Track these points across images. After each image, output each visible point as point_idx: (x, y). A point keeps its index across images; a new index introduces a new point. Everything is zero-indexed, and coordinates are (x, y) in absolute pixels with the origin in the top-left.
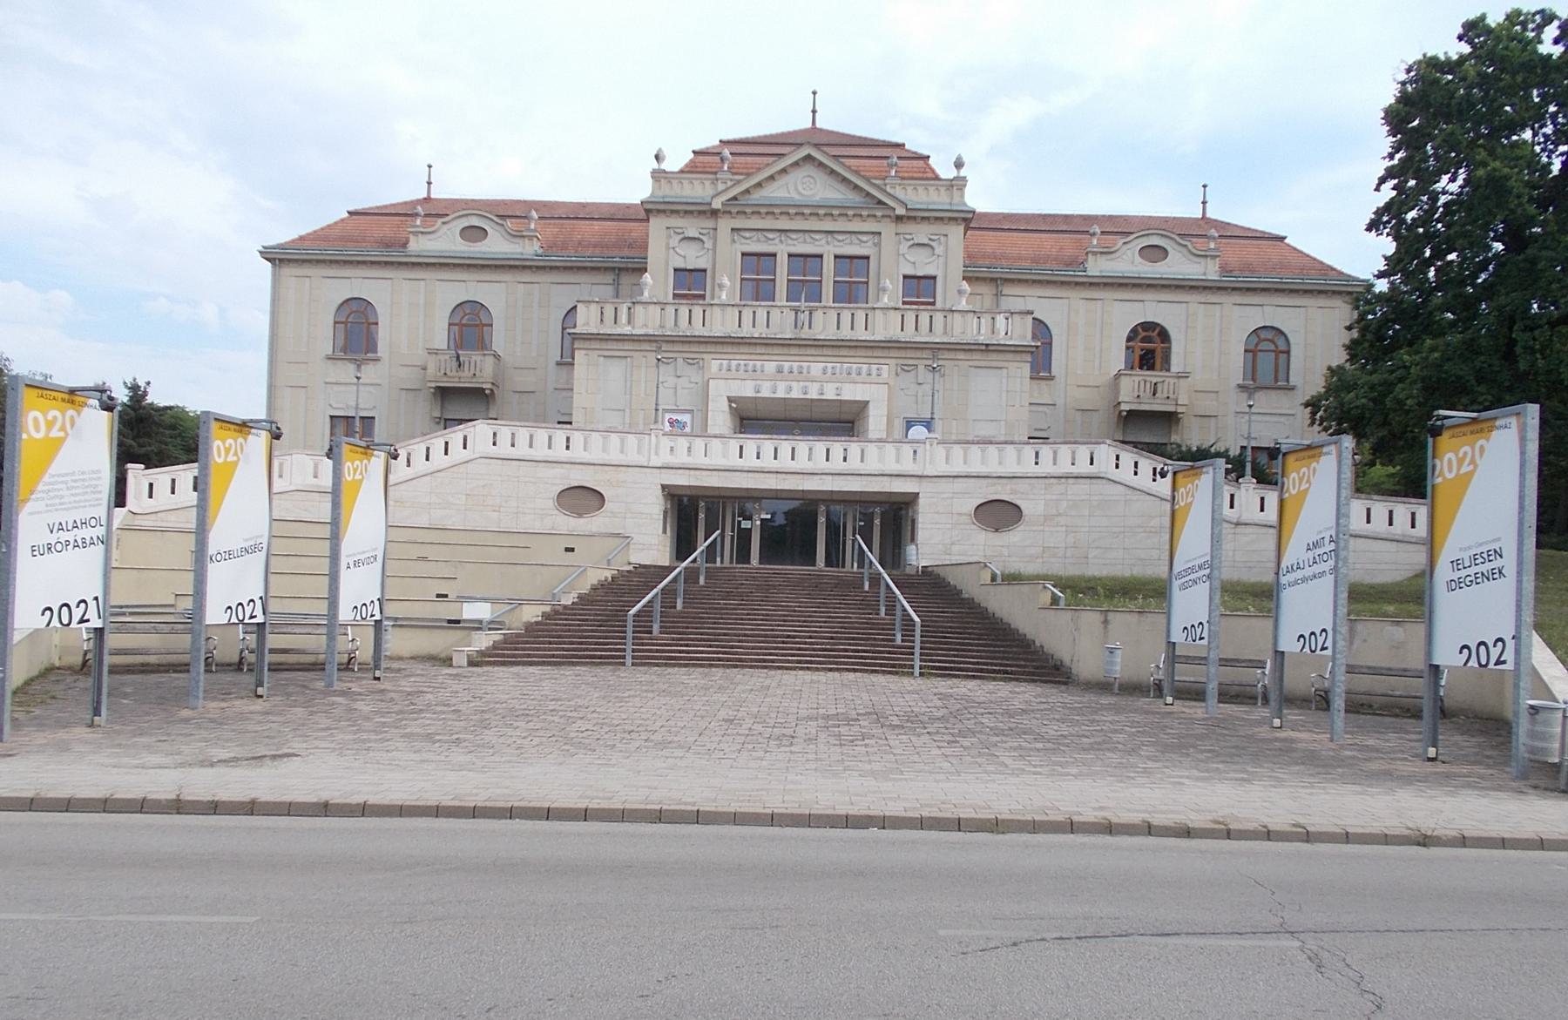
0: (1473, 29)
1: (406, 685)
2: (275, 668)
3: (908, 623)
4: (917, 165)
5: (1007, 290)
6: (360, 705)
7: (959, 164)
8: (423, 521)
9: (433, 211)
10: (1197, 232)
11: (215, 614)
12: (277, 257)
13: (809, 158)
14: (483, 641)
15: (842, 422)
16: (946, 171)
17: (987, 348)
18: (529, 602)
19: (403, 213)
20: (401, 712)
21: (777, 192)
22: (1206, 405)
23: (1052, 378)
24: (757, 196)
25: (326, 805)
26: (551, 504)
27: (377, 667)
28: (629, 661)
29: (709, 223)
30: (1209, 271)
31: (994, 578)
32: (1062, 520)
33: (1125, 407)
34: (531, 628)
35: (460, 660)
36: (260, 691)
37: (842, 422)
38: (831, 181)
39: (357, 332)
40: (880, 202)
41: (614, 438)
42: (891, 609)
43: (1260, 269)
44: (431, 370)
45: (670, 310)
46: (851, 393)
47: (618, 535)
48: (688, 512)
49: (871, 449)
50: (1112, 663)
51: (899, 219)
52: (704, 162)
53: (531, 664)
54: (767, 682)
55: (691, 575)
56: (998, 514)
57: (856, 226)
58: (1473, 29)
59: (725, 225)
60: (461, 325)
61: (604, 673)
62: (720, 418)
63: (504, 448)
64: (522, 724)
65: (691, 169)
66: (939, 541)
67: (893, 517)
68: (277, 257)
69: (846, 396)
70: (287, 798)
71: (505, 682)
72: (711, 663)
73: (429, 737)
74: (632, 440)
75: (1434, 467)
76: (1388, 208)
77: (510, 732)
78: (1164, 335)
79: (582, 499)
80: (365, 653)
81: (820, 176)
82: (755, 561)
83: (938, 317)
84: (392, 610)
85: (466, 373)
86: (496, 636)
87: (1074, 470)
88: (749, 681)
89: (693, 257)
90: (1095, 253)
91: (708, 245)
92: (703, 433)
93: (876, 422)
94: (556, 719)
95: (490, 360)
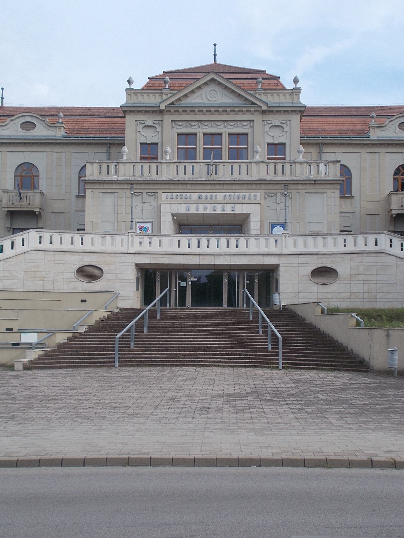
3: (275, 339)
4: (273, 82)
7: (296, 81)
14: (33, 355)
15: (235, 226)
16: (289, 85)
17: (315, 182)
21: (196, 99)
22: (57, 206)
23: (352, 197)
24: (184, 102)
28: (117, 364)
29: (159, 118)
30: (59, 134)
31: (323, 311)
33: (394, 212)
34: (61, 347)
35: (19, 366)
37: (235, 226)
40: (253, 103)
42: (265, 330)
45: (138, 166)
47: (111, 292)
48: (150, 278)
49: (252, 240)
50: (392, 360)
51: (264, 112)
52: (155, 84)
53: (60, 368)
54: (196, 374)
55: (152, 314)
56: (324, 275)
57: (240, 117)
59: (167, 118)
61: (103, 372)
62: (167, 225)
63: (46, 245)
64: (52, 405)
65: (148, 88)
66: (291, 290)
67: (265, 278)
71: (44, 378)
72: (163, 364)
77: (44, 410)
79: (90, 272)
85: (25, 203)
86: (40, 352)
89: (150, 137)
90: (374, 127)
91: (159, 129)
93: (254, 225)
95: (38, 196)
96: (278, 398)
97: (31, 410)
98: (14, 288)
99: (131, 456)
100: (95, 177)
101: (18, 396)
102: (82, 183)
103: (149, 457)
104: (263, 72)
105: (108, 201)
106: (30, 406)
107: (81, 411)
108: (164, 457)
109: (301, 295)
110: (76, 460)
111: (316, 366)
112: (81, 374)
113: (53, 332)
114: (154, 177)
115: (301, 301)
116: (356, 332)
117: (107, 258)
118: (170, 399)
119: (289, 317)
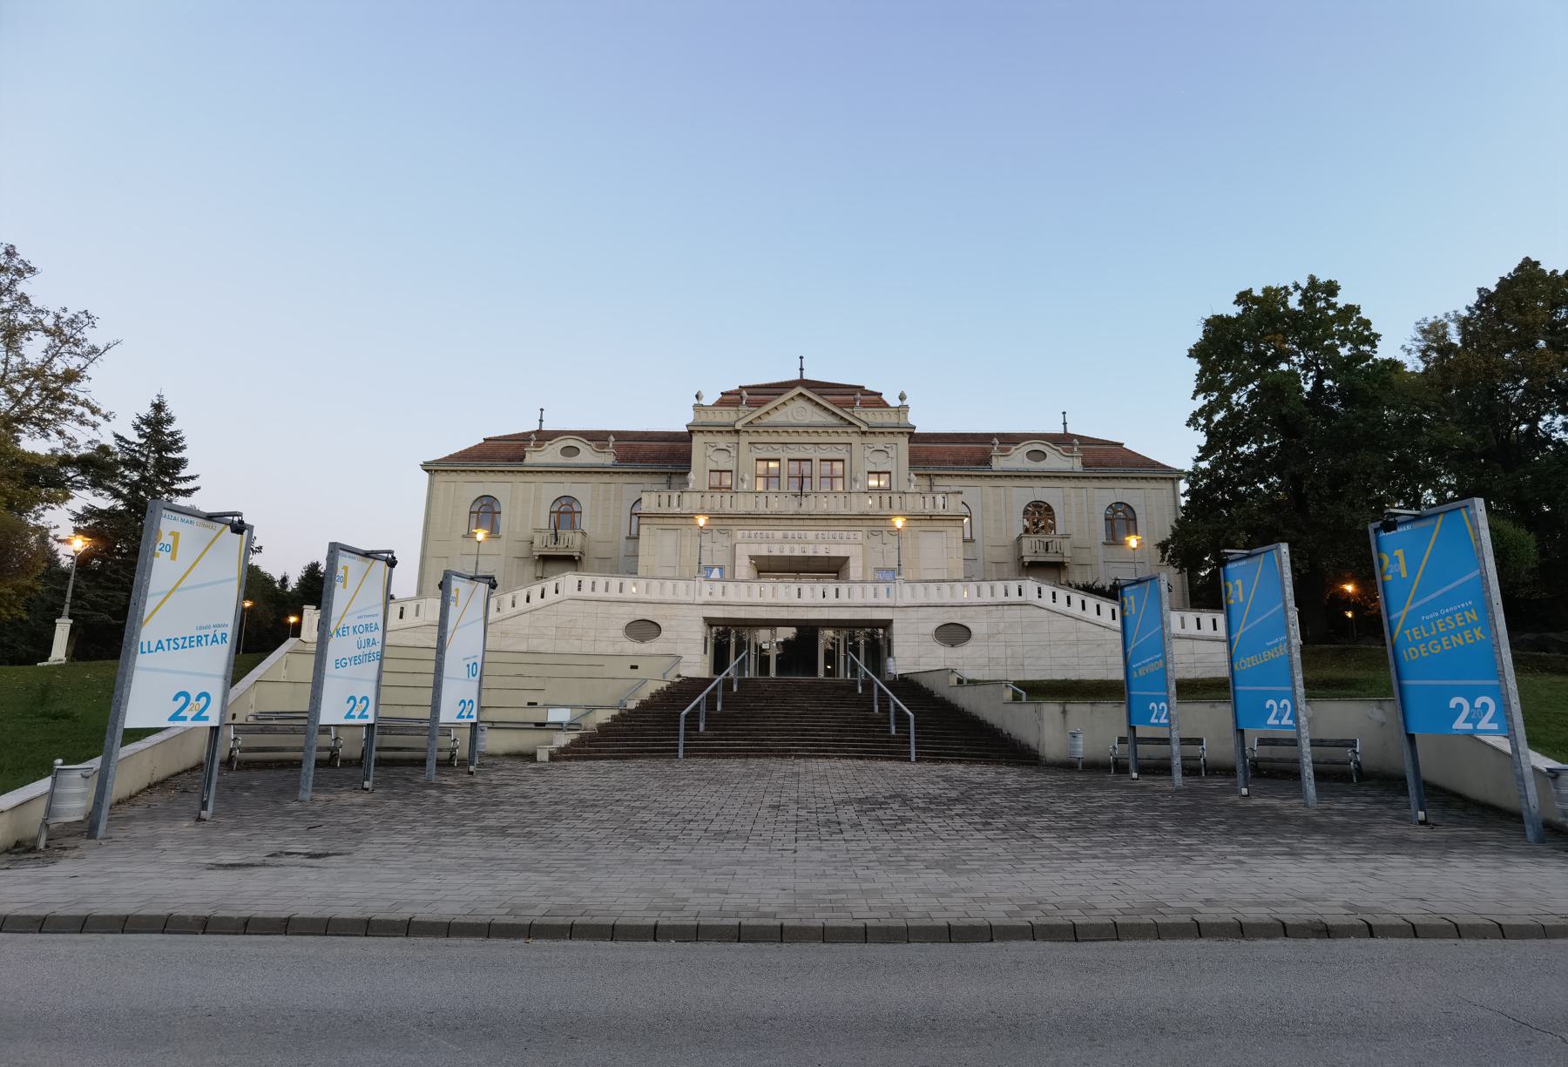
0: (1243, 297)
1: (494, 778)
2: (380, 763)
3: (901, 718)
4: (875, 400)
5: (938, 481)
6: (449, 798)
7: (902, 397)
8: (523, 648)
9: (543, 437)
10: (1063, 440)
11: (330, 714)
12: (431, 468)
13: (801, 395)
14: (563, 740)
15: (834, 568)
16: (893, 401)
17: (931, 518)
18: (602, 707)
19: (524, 438)
20: (483, 804)
21: (778, 417)
24: (766, 420)
25: (368, 922)
26: (621, 633)
27: (472, 763)
28: (681, 754)
29: (734, 439)
30: (608, 459)
31: (960, 681)
32: (1002, 637)
34: (603, 729)
35: (543, 755)
36: (367, 784)
37: (834, 568)
38: (816, 410)
39: (486, 511)
40: (851, 424)
41: (669, 584)
42: (884, 707)
43: (1107, 460)
44: (537, 542)
45: (708, 496)
46: (836, 551)
47: (670, 655)
48: (726, 636)
49: (857, 588)
50: (1075, 746)
51: (864, 433)
52: (730, 399)
53: (602, 758)
54: (796, 769)
55: (727, 684)
56: (953, 634)
57: (834, 439)
58: (1243, 297)
59: (744, 440)
60: (559, 512)
61: (662, 765)
62: (744, 568)
63: (587, 592)
64: (590, 815)
65: (720, 403)
66: (912, 654)
67: (873, 638)
68: (431, 468)
69: (833, 553)
70: (328, 913)
71: (579, 775)
72: (746, 754)
73: (503, 831)
74: (682, 585)
75: (1380, 560)
76: (1202, 410)
77: (578, 823)
78: (1049, 509)
79: (644, 629)
80: (463, 752)
81: (809, 407)
82: (773, 674)
83: (895, 498)
84: (490, 715)
85: (561, 545)
86: (574, 736)
87: (1007, 599)
88: (780, 768)
89: (723, 461)
91: (734, 453)
92: (733, 579)
93: (855, 570)
94: (622, 809)
95: (579, 536)
96: (935, 805)
97: (557, 825)
98: (542, 649)
99: (744, 922)
100: (654, 509)
101: (539, 799)
102: (635, 519)
103: (777, 923)
104: (861, 388)
105: (669, 539)
106: (555, 817)
107: (637, 826)
108: (805, 923)
109: (922, 660)
110: (639, 927)
111: (960, 758)
112: (631, 768)
113: (591, 709)
114: (728, 509)
115: (922, 668)
116: (1015, 708)
117: (667, 610)
118: (773, 807)
119: (908, 687)
